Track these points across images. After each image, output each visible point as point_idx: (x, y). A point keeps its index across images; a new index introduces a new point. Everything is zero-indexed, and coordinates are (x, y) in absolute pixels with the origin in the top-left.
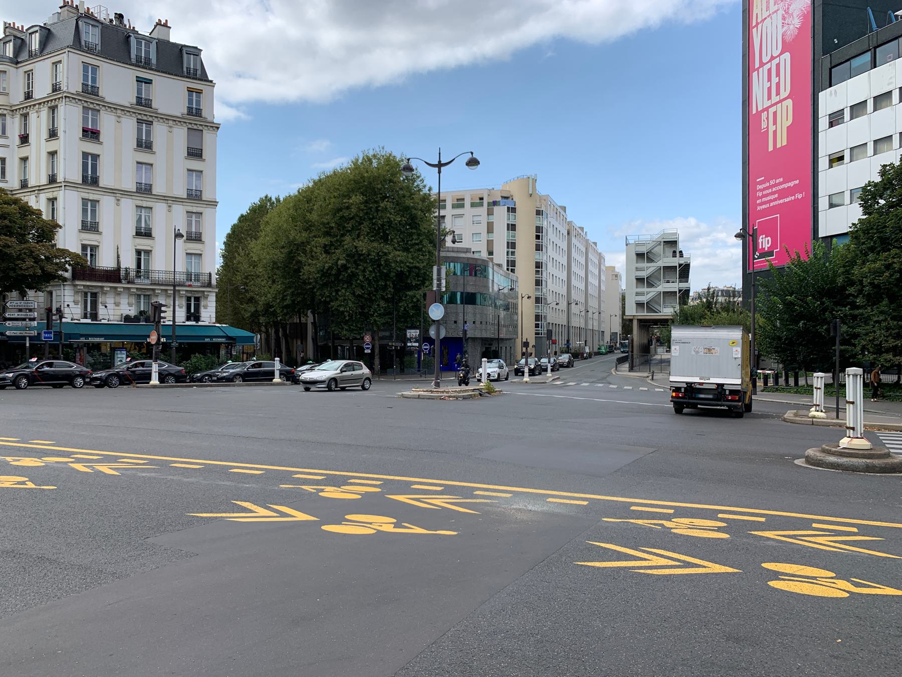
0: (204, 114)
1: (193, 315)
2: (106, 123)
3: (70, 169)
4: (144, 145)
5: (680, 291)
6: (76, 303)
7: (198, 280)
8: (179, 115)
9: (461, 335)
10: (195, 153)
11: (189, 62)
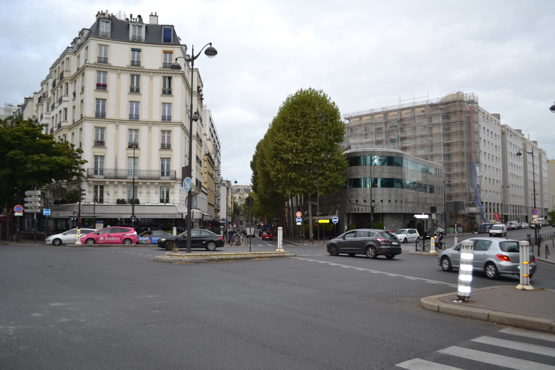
1: (165, 200)
2: (112, 79)
4: (135, 90)
6: (90, 192)
7: (102, 174)
8: (157, 68)
9: (369, 211)
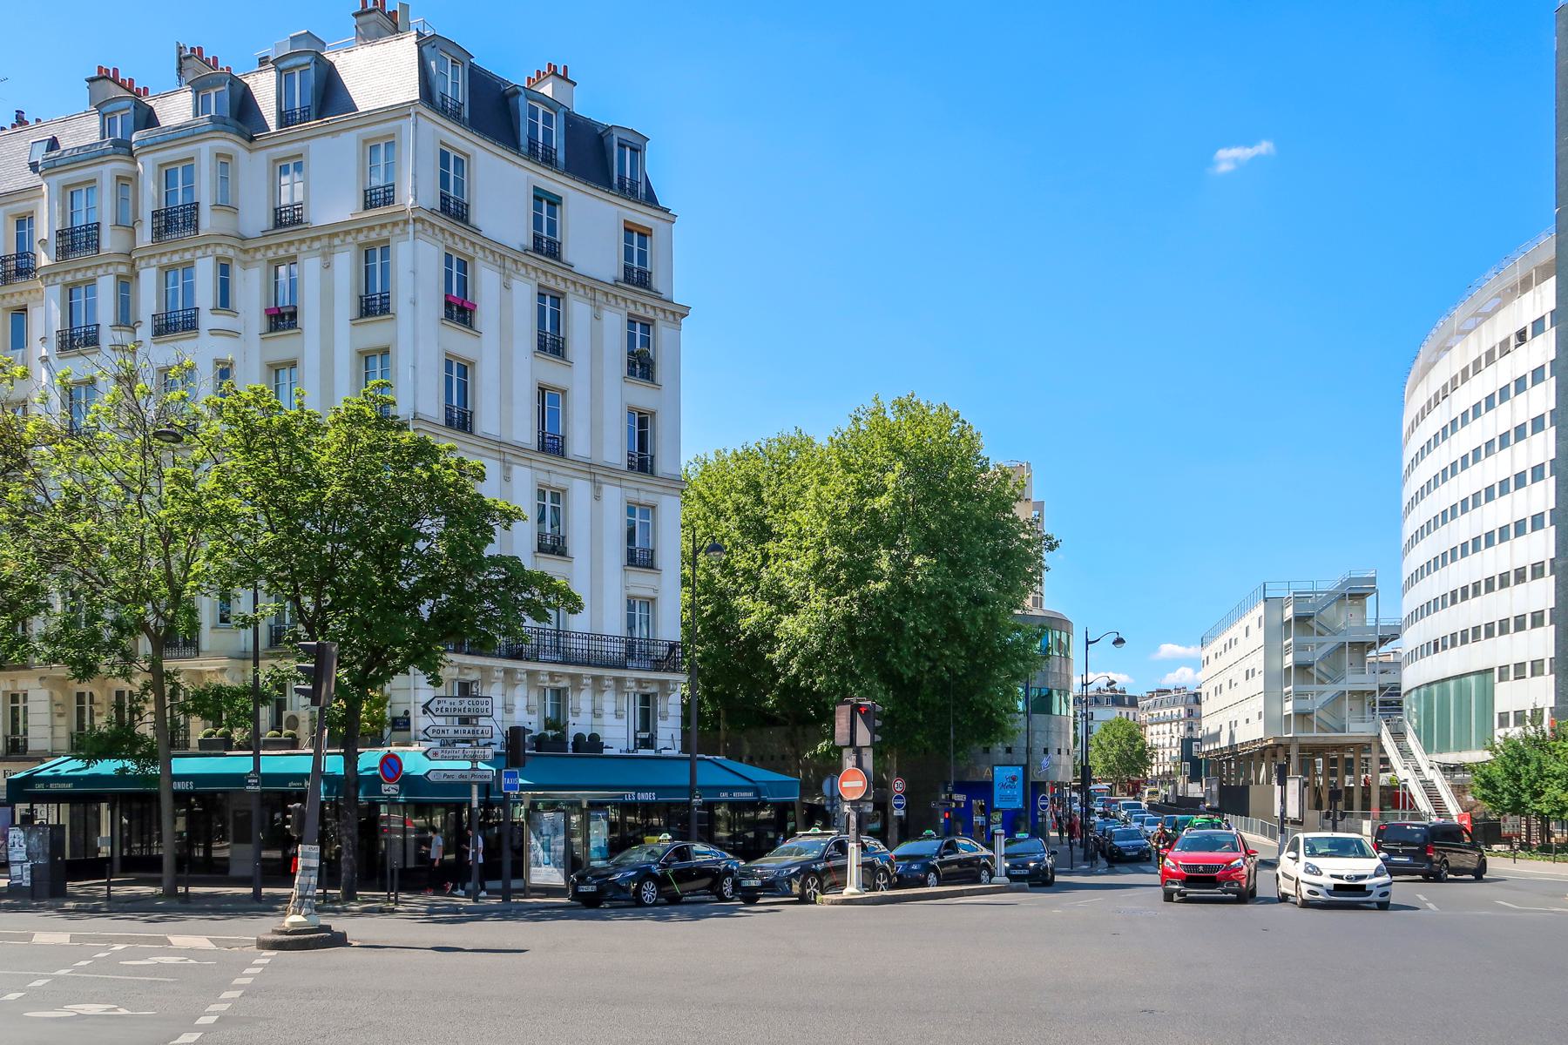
0: (657, 282)
3: (596, 431)
5: (1382, 689)
10: (641, 366)
11: (621, 164)
